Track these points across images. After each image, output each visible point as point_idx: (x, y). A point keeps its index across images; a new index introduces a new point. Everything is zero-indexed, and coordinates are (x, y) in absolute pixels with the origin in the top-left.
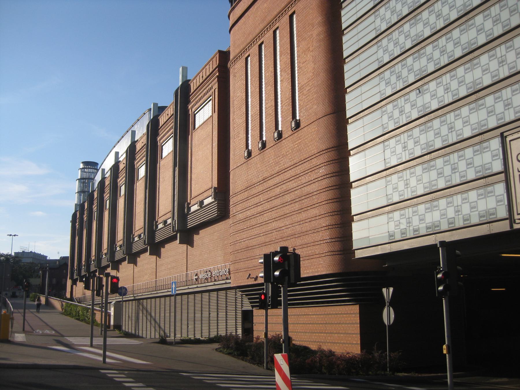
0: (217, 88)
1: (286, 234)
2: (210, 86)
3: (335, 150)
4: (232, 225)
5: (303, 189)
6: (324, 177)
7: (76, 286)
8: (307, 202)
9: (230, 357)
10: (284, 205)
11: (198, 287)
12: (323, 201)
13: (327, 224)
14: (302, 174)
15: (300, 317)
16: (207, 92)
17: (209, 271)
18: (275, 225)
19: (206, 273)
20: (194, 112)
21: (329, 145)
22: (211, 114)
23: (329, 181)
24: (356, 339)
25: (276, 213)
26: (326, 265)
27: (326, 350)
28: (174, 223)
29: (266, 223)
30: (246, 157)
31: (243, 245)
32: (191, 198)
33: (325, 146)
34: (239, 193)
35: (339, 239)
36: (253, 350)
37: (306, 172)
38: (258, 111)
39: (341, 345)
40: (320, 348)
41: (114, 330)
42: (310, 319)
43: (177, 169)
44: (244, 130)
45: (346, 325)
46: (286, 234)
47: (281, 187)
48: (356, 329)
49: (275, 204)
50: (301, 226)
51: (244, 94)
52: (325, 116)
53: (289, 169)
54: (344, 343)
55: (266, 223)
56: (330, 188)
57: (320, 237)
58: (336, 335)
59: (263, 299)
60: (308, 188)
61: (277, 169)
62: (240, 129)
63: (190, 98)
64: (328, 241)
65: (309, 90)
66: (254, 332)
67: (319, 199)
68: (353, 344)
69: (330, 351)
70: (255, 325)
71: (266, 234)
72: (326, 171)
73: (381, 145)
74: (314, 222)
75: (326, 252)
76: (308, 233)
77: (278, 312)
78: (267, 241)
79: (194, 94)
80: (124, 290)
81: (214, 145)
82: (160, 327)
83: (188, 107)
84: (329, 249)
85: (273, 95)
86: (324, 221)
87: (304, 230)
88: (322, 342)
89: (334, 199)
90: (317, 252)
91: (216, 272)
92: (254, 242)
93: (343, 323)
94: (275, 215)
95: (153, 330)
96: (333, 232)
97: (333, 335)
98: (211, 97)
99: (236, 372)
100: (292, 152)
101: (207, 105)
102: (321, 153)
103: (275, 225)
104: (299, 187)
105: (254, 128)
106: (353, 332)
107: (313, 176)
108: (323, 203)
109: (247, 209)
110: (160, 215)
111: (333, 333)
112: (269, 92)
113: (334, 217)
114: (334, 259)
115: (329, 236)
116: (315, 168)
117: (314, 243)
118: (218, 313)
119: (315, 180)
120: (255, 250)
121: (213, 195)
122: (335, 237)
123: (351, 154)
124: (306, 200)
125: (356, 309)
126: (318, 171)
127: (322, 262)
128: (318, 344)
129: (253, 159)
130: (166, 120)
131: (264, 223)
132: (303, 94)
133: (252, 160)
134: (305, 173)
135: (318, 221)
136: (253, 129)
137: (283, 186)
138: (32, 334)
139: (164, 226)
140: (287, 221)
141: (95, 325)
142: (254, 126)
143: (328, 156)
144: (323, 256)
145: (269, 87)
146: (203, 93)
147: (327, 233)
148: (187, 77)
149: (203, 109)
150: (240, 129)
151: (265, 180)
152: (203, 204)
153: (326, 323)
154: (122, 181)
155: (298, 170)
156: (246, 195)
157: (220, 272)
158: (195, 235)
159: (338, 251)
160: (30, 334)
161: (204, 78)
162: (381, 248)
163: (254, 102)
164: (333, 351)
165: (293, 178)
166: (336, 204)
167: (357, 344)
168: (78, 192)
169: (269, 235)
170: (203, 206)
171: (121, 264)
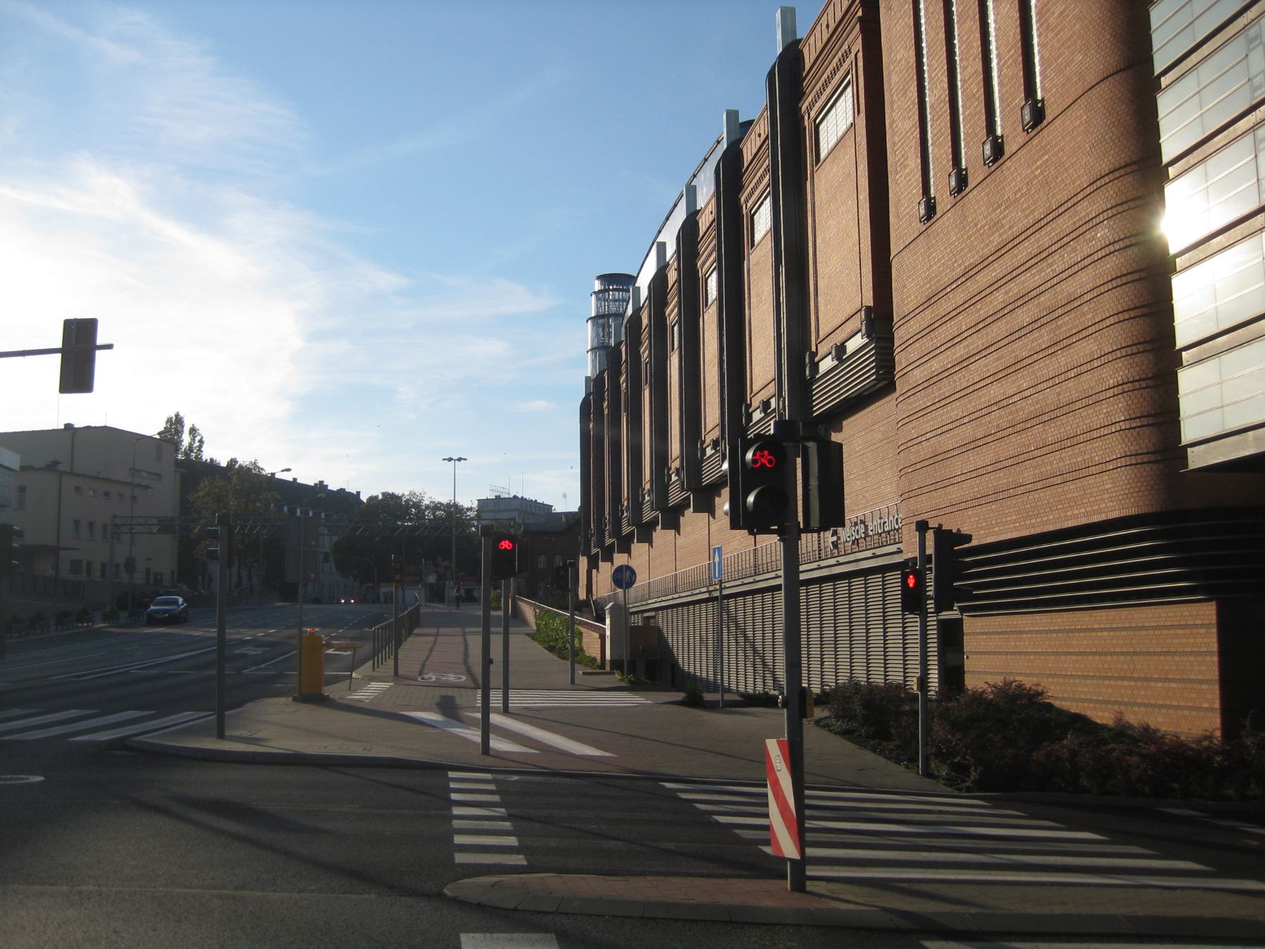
0: (861, 50)
1: (1021, 413)
2: (845, 47)
3: (1135, 171)
4: (900, 399)
5: (1058, 288)
6: (1107, 250)
7: (598, 570)
8: (1068, 324)
9: (843, 740)
10: (1016, 335)
11: (839, 564)
12: (1108, 315)
13: (1119, 378)
14: (1054, 248)
15: (1071, 635)
16: (841, 63)
17: (863, 522)
18: (995, 392)
19: (853, 528)
20: (815, 120)
21: (1118, 158)
22: (850, 120)
23: (1122, 260)
24: (1210, 696)
25: (999, 359)
26: (1118, 493)
27: (1136, 724)
28: (781, 406)
29: (975, 388)
30: (922, 218)
31: (925, 450)
32: (819, 340)
33: (1108, 163)
34: (912, 315)
35: (1151, 420)
36: (904, 724)
37: (1062, 243)
38: (944, 91)
39: (1171, 712)
40: (1120, 720)
41: (611, 673)
42: (1097, 642)
43: (783, 270)
44: (916, 149)
45: (1185, 658)
46: (1021, 413)
47: (1007, 288)
48: (1209, 668)
49: (994, 335)
50: (1058, 390)
51: (912, 52)
52: (1105, 79)
53: (1023, 237)
54: (1179, 707)
55: (975, 388)
56: (1124, 280)
57: (1103, 416)
58: (1159, 684)
59: (911, 585)
60: (1069, 283)
61: (996, 240)
62: (907, 145)
63: (804, 84)
64: (1123, 427)
65: (1061, 13)
66: (966, 675)
67: (1098, 312)
68: (1200, 709)
69: (1146, 729)
70: (967, 658)
71: (975, 417)
72: (1113, 232)
73: (1248, 139)
74: (1087, 376)
75: (1119, 456)
76: (1073, 407)
77: (1020, 622)
78: (979, 435)
79: (810, 75)
80: (628, 573)
81: (861, 197)
82: (764, 664)
83: (801, 108)
84: (1127, 449)
85: (977, 43)
86: (1111, 373)
87: (1064, 401)
88: (1125, 704)
89: (1135, 308)
90: (1097, 458)
91: (875, 523)
92: (949, 441)
93: (1175, 653)
94: (994, 365)
95: (750, 669)
96: (1136, 401)
97: (1152, 684)
98: (850, 76)
99: (827, 783)
100: (1029, 190)
101: (843, 98)
102: (1098, 184)
103: (995, 392)
104: (1049, 285)
105: (938, 139)
106: (1201, 677)
107: (1083, 248)
108: (1108, 322)
109: (931, 355)
110: (755, 389)
111: (1151, 679)
112: (968, 38)
113: (1136, 360)
114: (1139, 475)
115: (1126, 413)
116: (1084, 228)
117: (1088, 434)
118: (885, 629)
119: (1086, 262)
120: (953, 461)
121: (864, 328)
122: (1139, 415)
123: (1171, 176)
124: (1066, 318)
125: (1208, 612)
126: (1093, 234)
127: (1110, 486)
128: (1116, 707)
129: (941, 221)
130: (757, 148)
131: (971, 389)
132: (1048, 26)
133: (937, 224)
134: (1062, 243)
135: (1096, 373)
136: (936, 141)
137: (1012, 284)
138: (412, 682)
139: (763, 415)
140: (1023, 380)
141: (577, 663)
142: (938, 132)
143: (1117, 190)
144: (1111, 468)
145: (969, 23)
146: (831, 67)
147: (1120, 405)
148: (794, 32)
149: (834, 110)
150: (907, 145)
151: (969, 274)
152: (845, 353)
153: (1135, 653)
154: (672, 313)
155: (1045, 238)
156: (927, 317)
157: (885, 523)
158: (833, 434)
159: (1148, 453)
160: (407, 682)
161: (831, 30)
162: (1256, 439)
163: (935, 70)
164: (1152, 727)
165: (1033, 262)
166: (1141, 322)
167: (1212, 709)
168: (591, 350)
169: (983, 420)
170: (844, 357)
171: (683, 516)
